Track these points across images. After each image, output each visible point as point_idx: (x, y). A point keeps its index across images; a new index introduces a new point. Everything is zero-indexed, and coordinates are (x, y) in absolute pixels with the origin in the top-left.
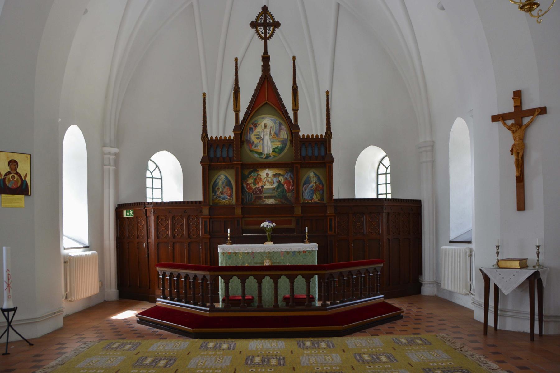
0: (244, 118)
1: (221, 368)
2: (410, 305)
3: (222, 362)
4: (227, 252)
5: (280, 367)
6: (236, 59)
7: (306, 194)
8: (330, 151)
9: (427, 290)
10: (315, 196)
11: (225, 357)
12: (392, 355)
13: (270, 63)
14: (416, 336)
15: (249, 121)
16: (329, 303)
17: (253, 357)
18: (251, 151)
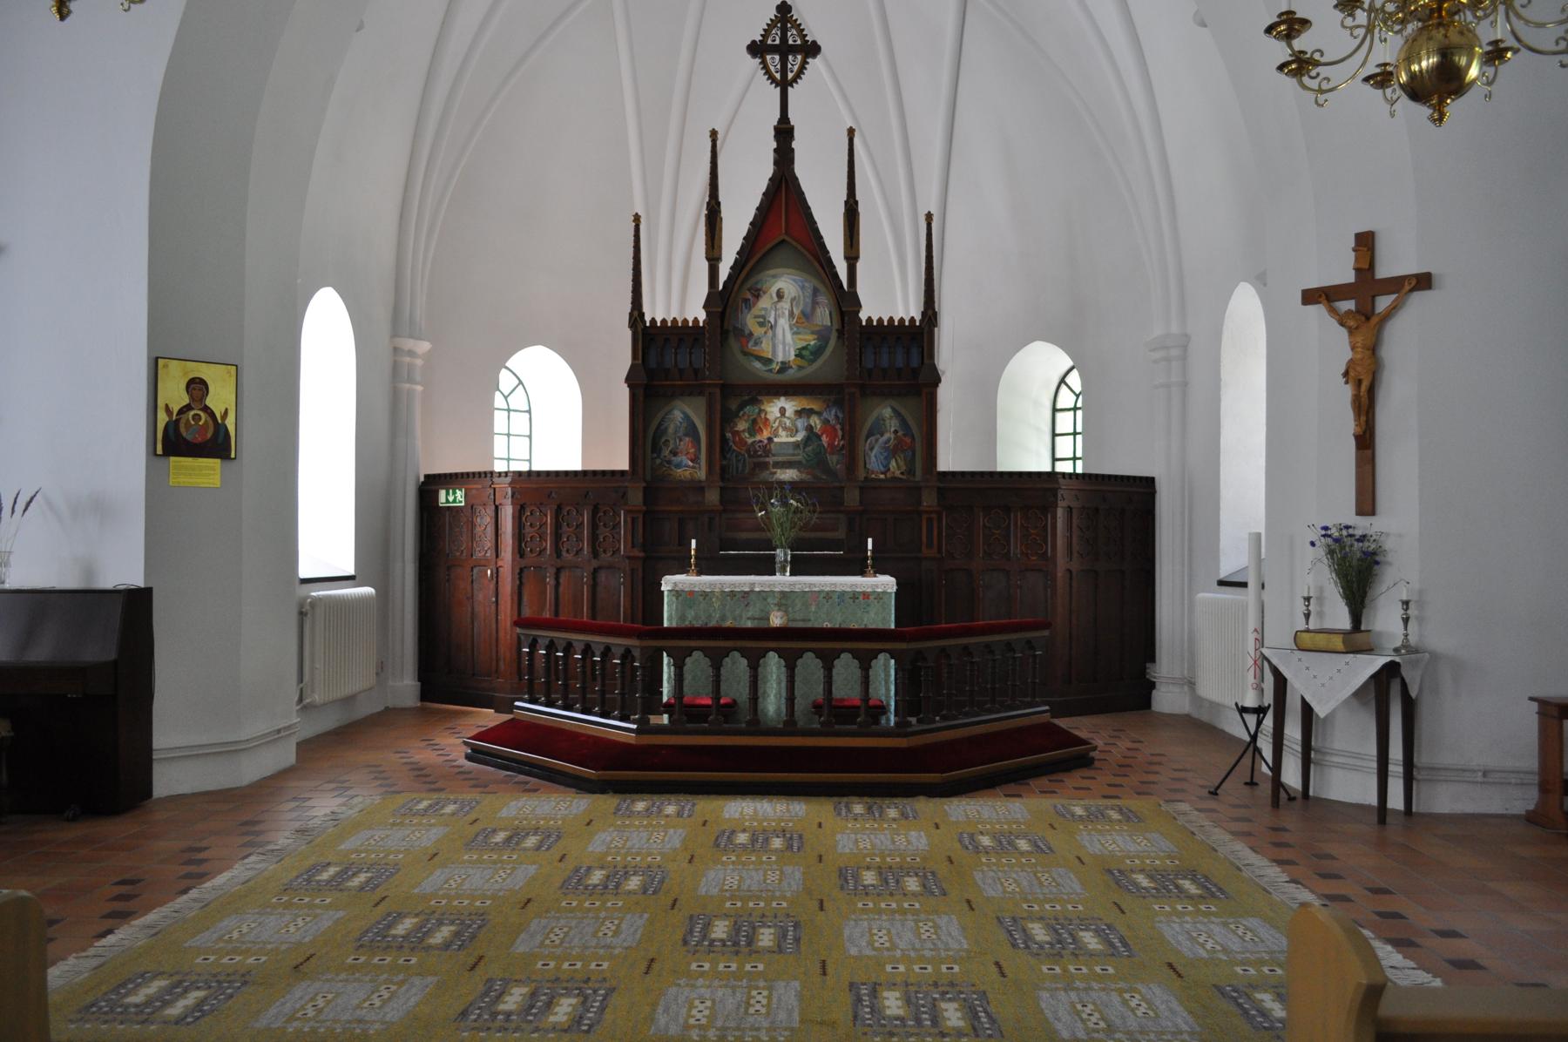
6: (714, 134)
8: (932, 356)
9: (1167, 699)
10: (893, 463)
12: (1043, 839)
13: (794, 145)
16: (913, 720)
17: (733, 832)
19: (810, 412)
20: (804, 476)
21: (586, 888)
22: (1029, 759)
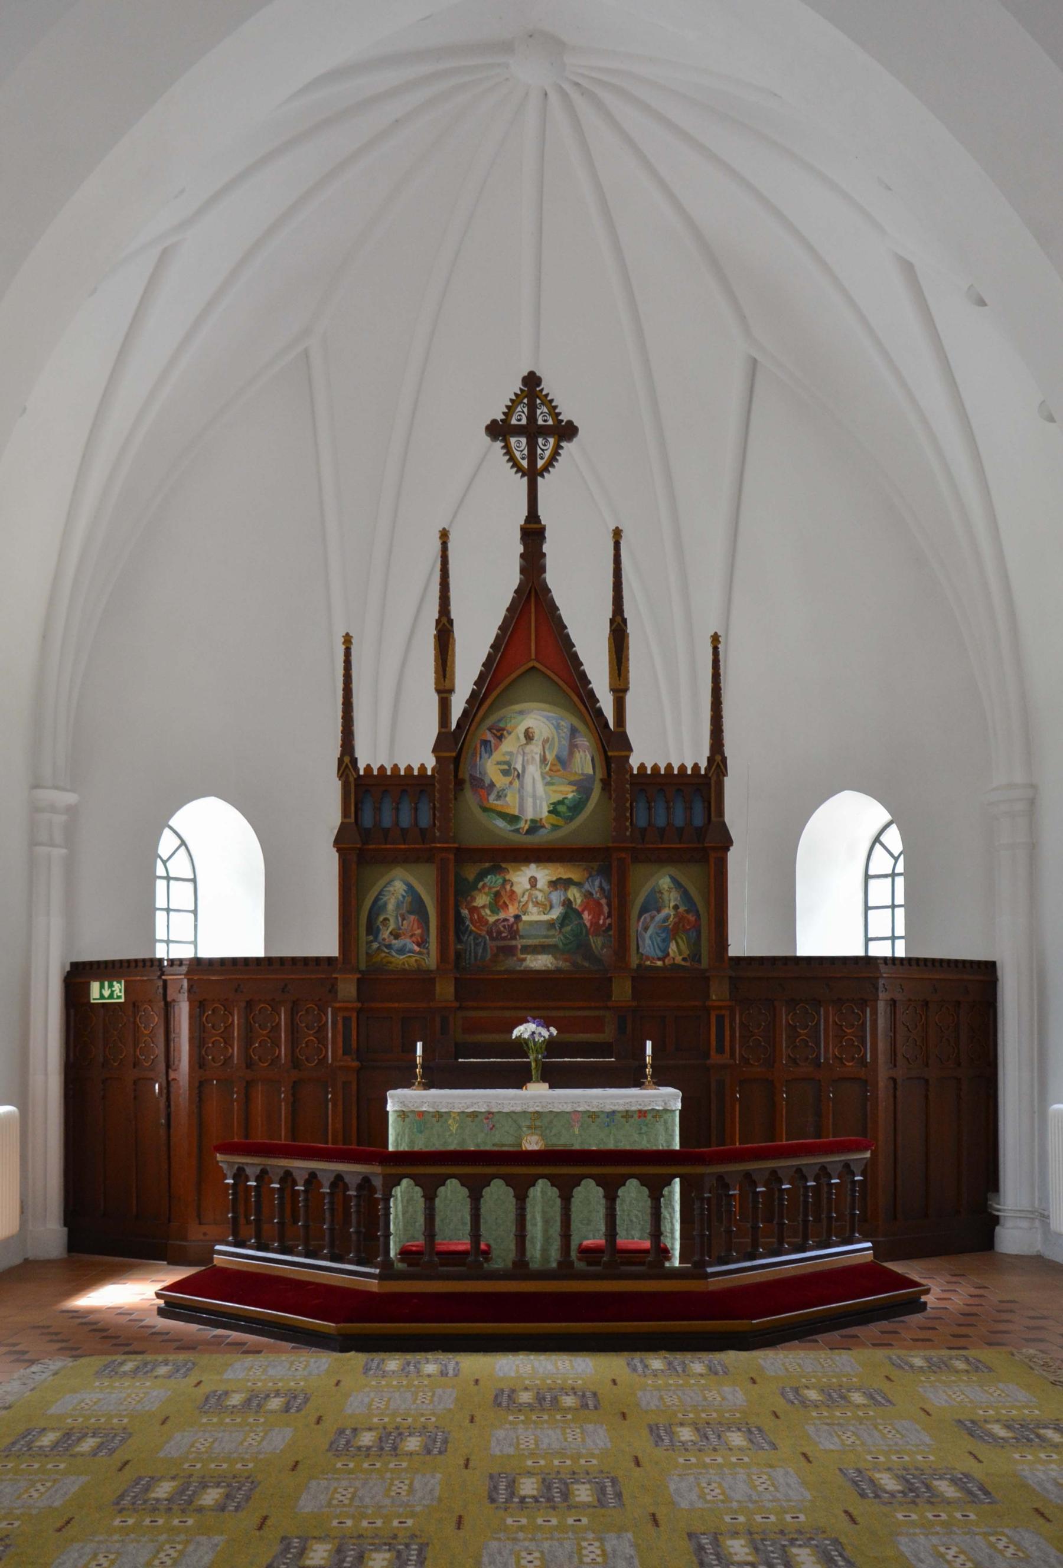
0: (465, 713)
1: (434, 1414)
2: (954, 1279)
3: (432, 1401)
4: (409, 1108)
5: (586, 1412)
7: (648, 941)
8: (721, 813)
9: (1012, 1238)
10: (673, 946)
11: (439, 1391)
13: (546, 548)
14: (953, 1353)
15: (483, 719)
18: (485, 810)
19: (567, 883)
20: (561, 964)
21: (359, 1448)
22: (858, 1305)
